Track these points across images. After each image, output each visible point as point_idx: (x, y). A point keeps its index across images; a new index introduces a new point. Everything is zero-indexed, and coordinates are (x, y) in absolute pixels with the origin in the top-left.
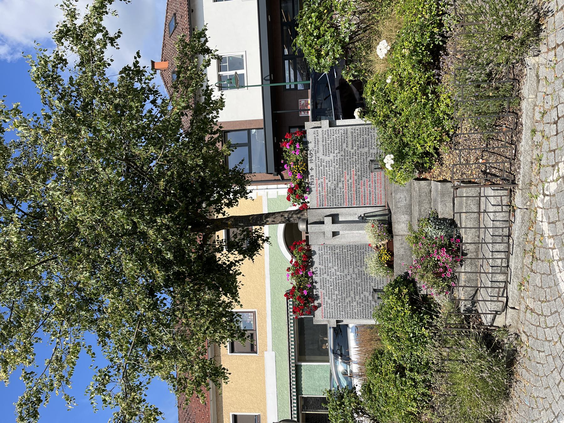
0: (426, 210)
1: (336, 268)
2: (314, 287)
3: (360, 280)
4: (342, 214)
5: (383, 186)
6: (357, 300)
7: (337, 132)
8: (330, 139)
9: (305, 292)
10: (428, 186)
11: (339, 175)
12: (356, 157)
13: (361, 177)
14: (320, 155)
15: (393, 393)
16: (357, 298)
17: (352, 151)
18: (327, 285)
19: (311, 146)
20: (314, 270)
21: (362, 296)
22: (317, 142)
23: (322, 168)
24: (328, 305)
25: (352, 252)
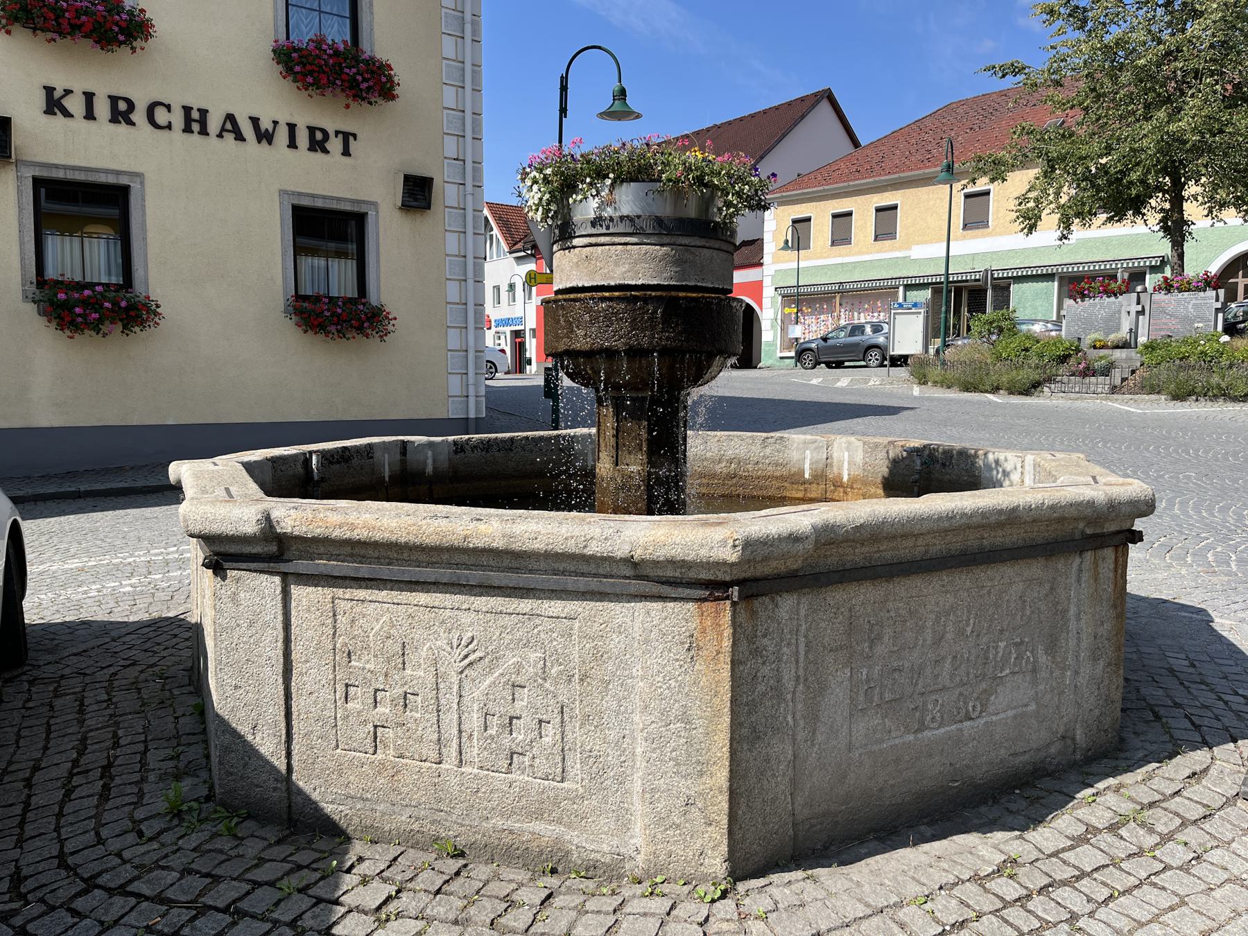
14: (1194, 301)
15: (1012, 346)
19: (1202, 294)
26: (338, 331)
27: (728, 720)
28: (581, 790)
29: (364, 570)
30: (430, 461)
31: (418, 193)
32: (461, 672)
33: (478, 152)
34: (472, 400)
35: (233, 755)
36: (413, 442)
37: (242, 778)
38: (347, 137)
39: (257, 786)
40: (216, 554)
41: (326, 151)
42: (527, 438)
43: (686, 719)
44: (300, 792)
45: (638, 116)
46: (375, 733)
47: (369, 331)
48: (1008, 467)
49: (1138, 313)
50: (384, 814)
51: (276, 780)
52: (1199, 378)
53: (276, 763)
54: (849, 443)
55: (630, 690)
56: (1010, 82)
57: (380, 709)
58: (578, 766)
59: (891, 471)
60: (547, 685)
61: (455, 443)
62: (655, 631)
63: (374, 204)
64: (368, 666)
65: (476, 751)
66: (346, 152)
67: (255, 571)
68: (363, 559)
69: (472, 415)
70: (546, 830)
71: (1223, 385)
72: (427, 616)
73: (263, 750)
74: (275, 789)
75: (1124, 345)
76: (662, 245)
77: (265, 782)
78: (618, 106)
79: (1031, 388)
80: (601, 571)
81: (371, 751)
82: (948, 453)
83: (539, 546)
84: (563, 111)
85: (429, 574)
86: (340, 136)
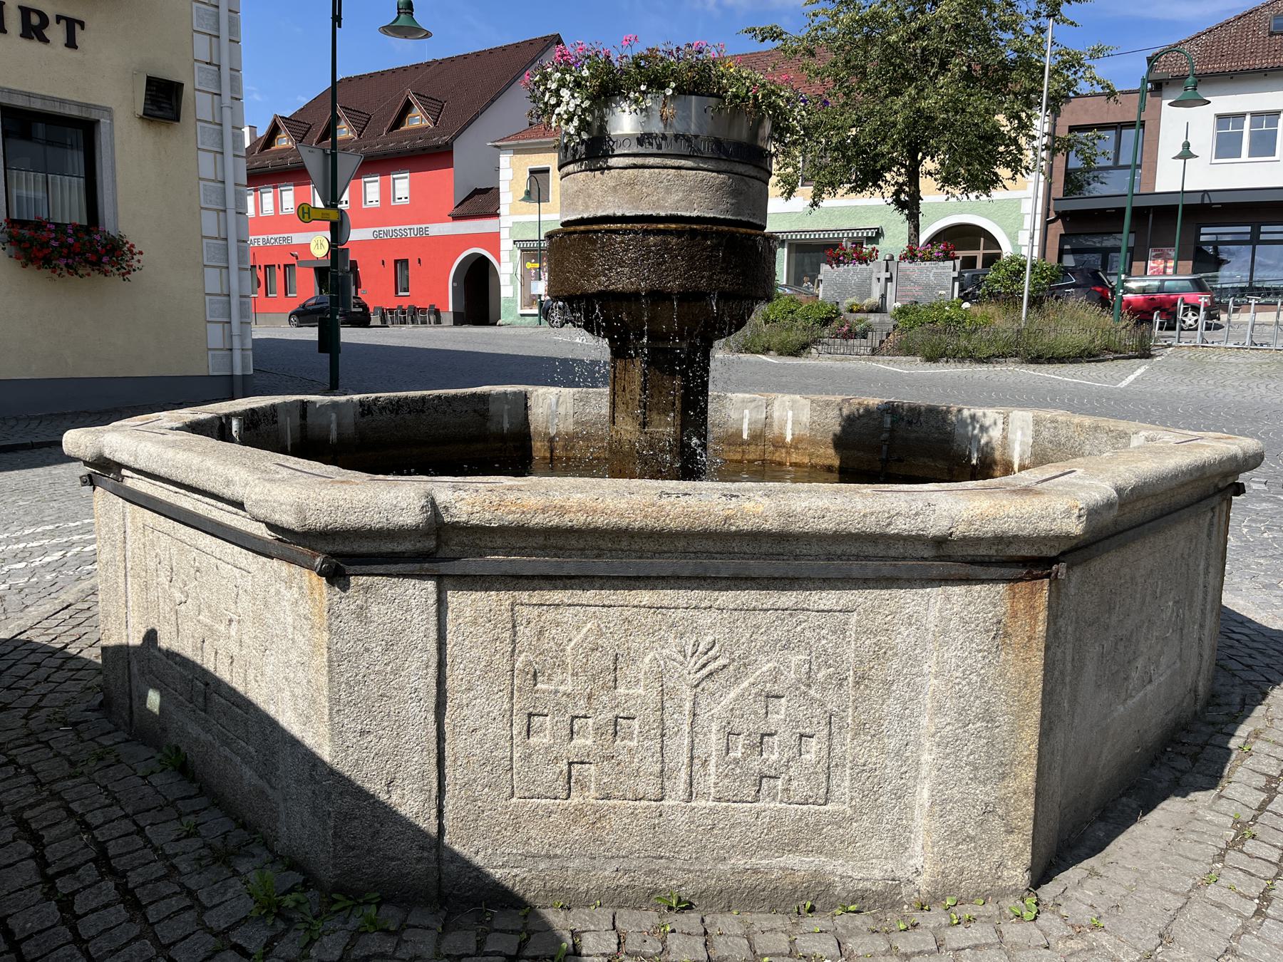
22: (944, 268)
26: (67, 265)
27: (1038, 713)
28: (849, 812)
29: (570, 565)
30: (334, 426)
31: (163, 100)
32: (697, 686)
33: (235, 56)
34: (237, 355)
35: (356, 823)
36: (314, 403)
37: (369, 851)
38: (72, 25)
39: (392, 859)
40: (333, 555)
41: (45, 40)
42: (439, 397)
43: (988, 716)
44: (455, 857)
45: (428, 35)
46: (570, 772)
47: (108, 267)
48: (987, 422)
49: (888, 280)
50: (578, 871)
51: (422, 848)
52: (952, 342)
53: (424, 826)
54: (794, 402)
55: (917, 691)
56: (769, 45)
57: (578, 741)
58: (847, 783)
59: (844, 429)
60: (812, 692)
61: (361, 403)
62: (955, 620)
63: (108, 110)
64: (562, 688)
65: (713, 779)
66: (71, 43)
67: (398, 576)
68: (559, 551)
69: (238, 372)
70: (801, 863)
71: (970, 348)
72: (650, 619)
73: (403, 811)
74: (419, 860)
75: (879, 309)
76: (718, 172)
77: (404, 852)
78: (404, 20)
79: (798, 350)
80: (892, 553)
81: (564, 795)
82: (915, 411)
83: (827, 525)
84: (337, 19)
85: (664, 565)
86: (63, 22)
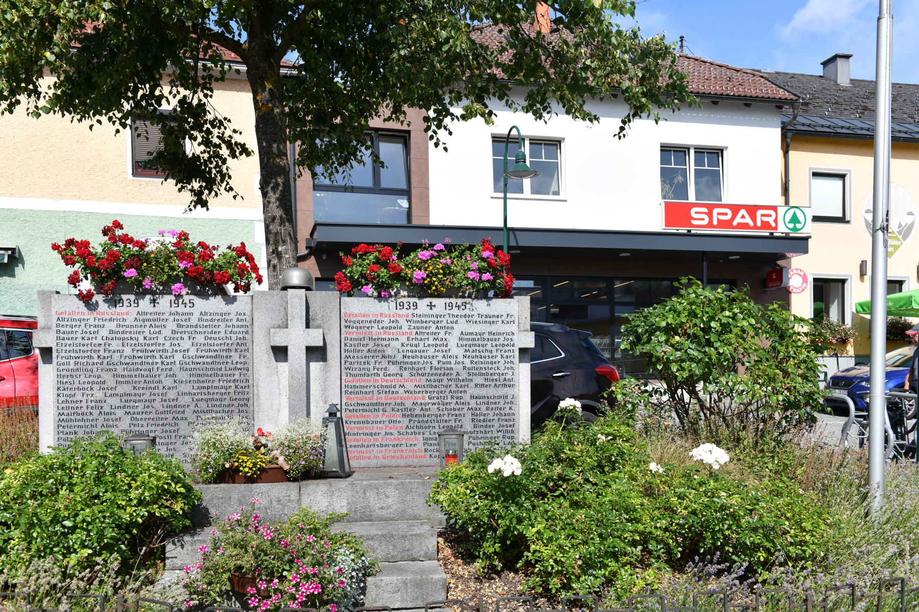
0: (377, 552)
1: (193, 352)
2: (141, 294)
3: (161, 409)
4: (325, 371)
5: (387, 462)
6: (109, 400)
7: (509, 365)
8: (494, 349)
9: (131, 273)
10: (426, 553)
11: (416, 366)
12: (453, 406)
13: (408, 414)
14: (463, 326)
16: (115, 401)
17: (467, 397)
18: (147, 330)
20: (187, 298)
21: (120, 413)
22: (490, 319)
23: (433, 329)
24: (92, 329)
25: (231, 390)
